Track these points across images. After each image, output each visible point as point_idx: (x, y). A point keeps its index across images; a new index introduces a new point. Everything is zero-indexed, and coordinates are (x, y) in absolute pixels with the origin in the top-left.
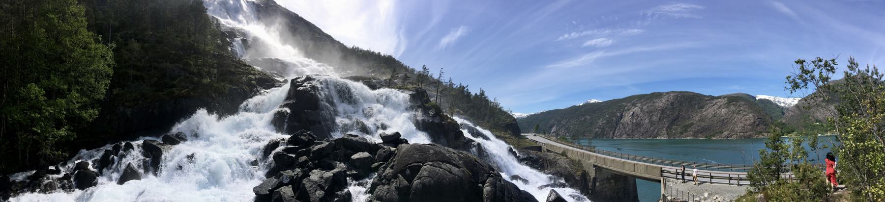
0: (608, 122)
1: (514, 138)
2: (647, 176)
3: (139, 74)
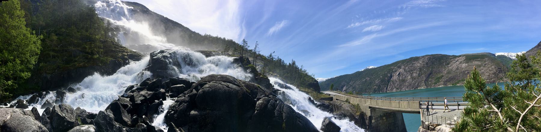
1: (314, 92)
3: (56, 54)
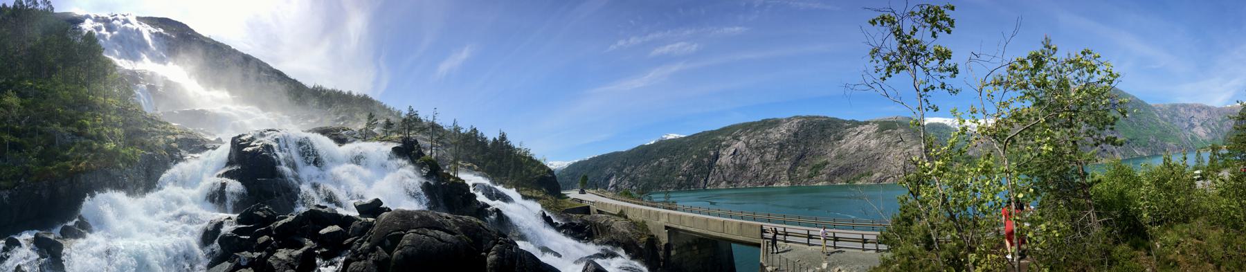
0: (696, 166)
2: (741, 238)
3: (18, 140)
